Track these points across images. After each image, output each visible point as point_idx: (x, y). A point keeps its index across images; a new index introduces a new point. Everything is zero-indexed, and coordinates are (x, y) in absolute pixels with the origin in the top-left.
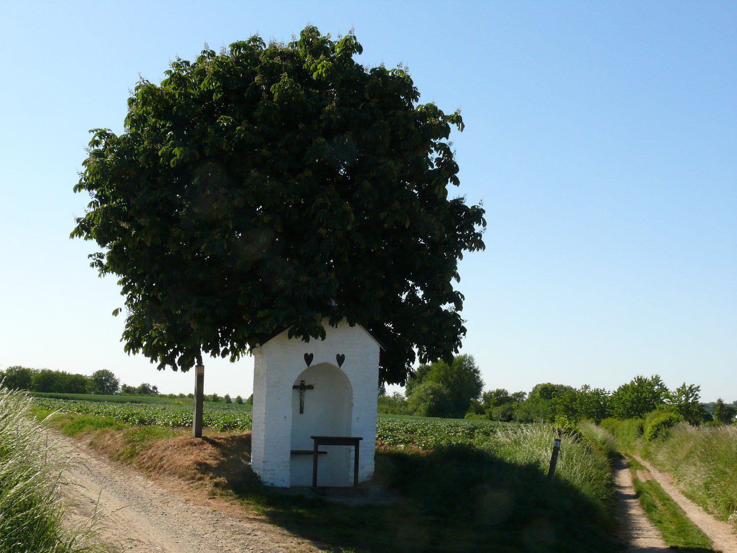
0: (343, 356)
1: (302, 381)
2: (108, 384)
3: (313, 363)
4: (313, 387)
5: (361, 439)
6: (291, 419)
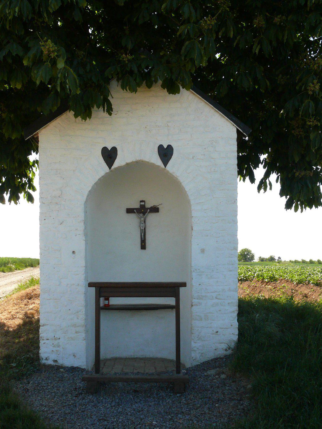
0: (170, 148)
1: (141, 201)
2: (249, 257)
3: (117, 163)
4: (35, 191)
5: (184, 285)
6: (83, 254)
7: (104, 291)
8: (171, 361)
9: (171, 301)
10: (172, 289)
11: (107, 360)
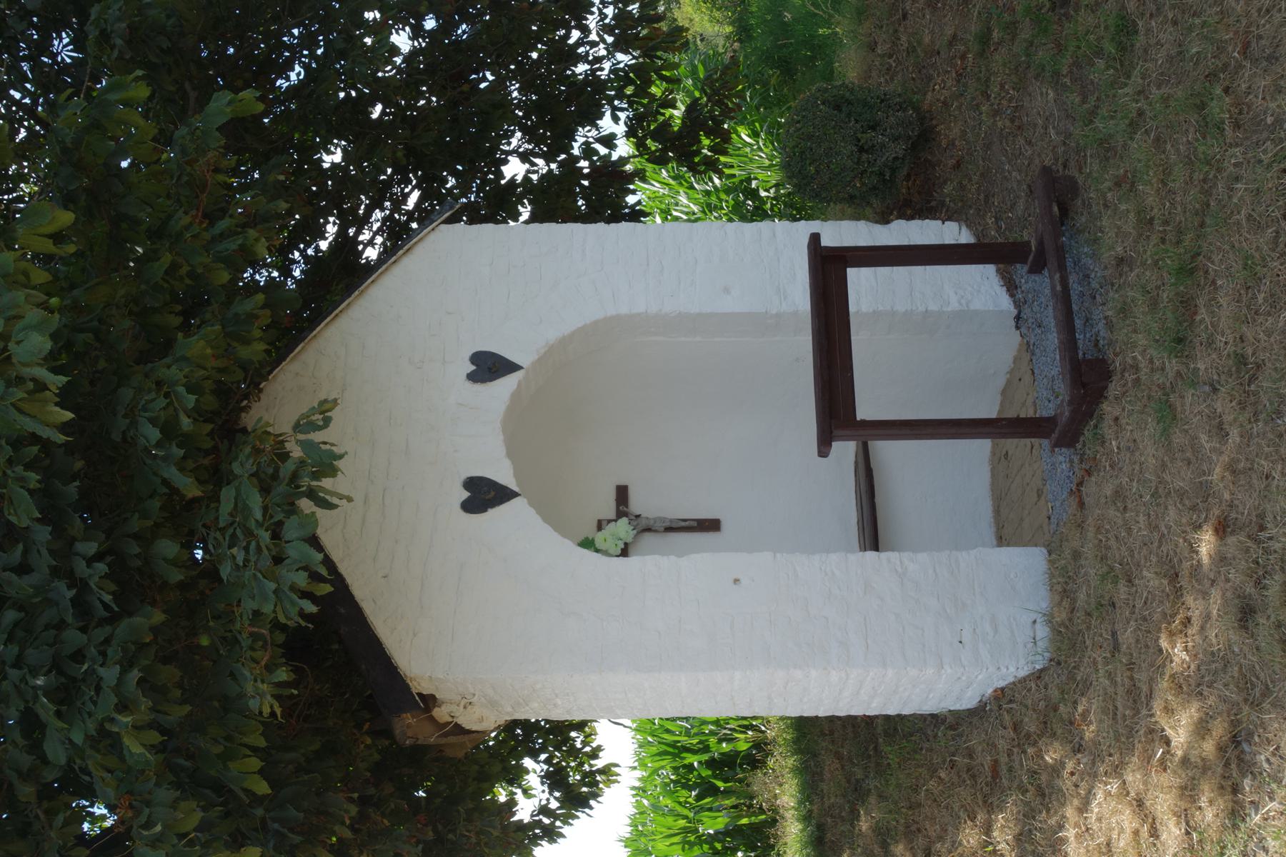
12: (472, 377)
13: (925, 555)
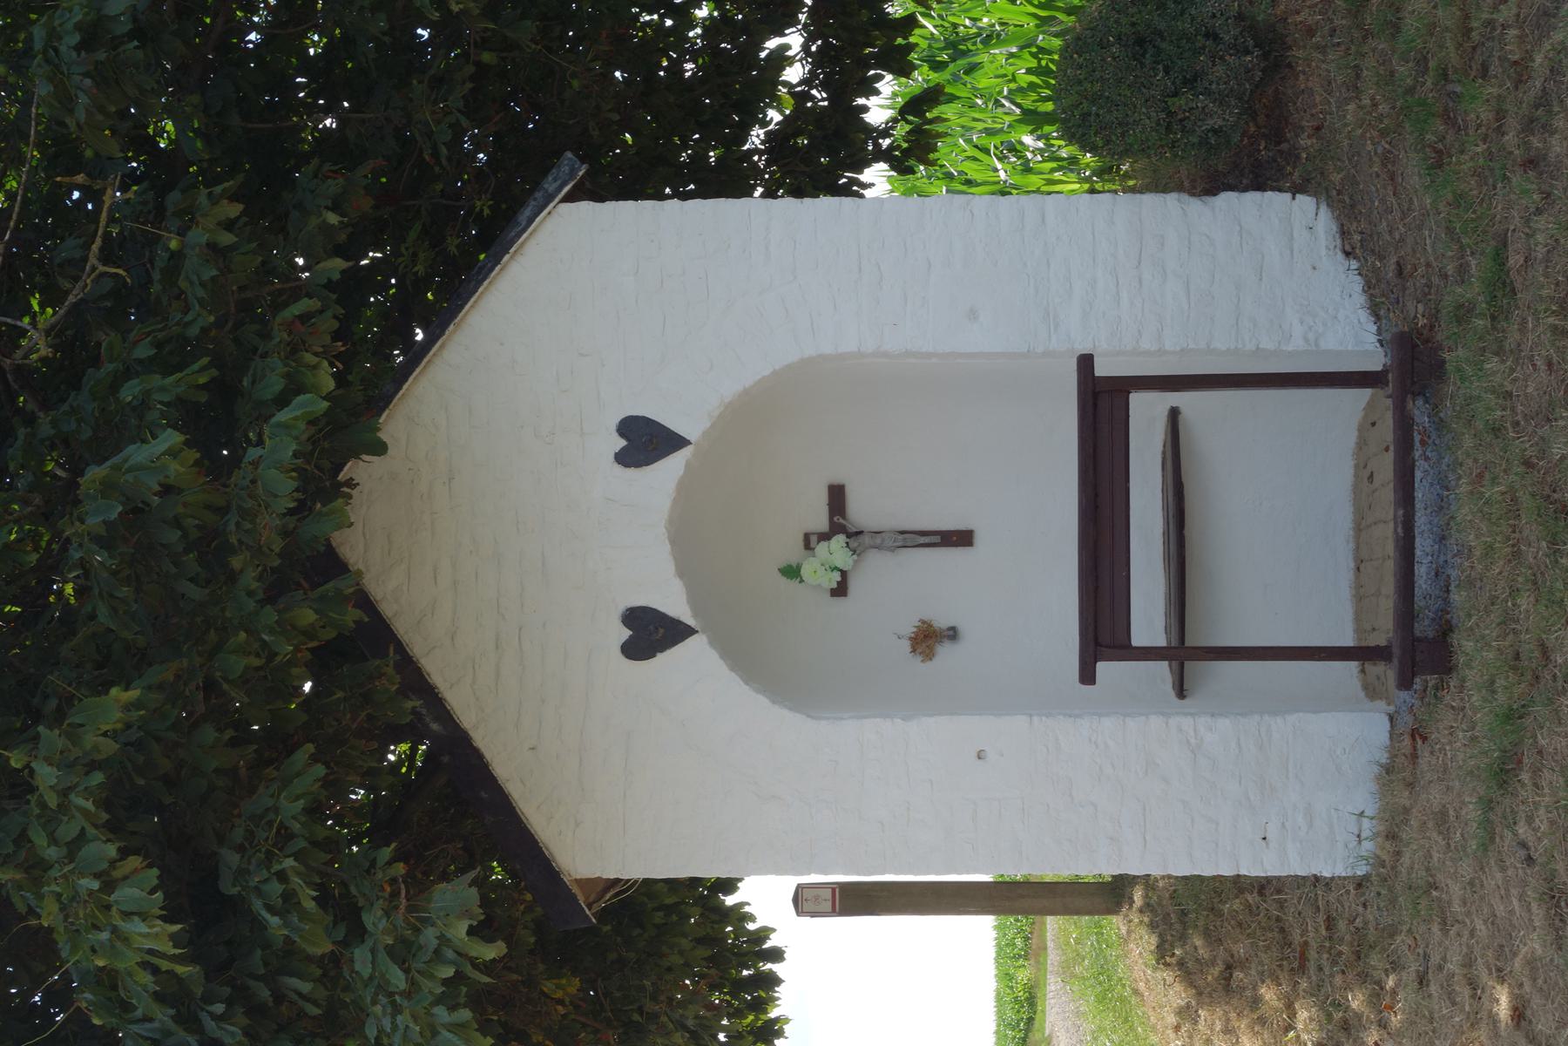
3: (675, 605)
7: (1103, 634)
8: (1017, 956)
9: (1146, 411)
10: (1102, 401)
11: (1359, 631)
12: (623, 459)
13: (1227, 721)
